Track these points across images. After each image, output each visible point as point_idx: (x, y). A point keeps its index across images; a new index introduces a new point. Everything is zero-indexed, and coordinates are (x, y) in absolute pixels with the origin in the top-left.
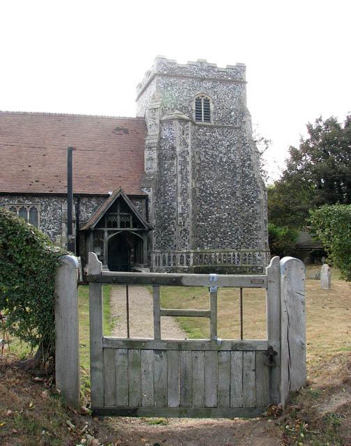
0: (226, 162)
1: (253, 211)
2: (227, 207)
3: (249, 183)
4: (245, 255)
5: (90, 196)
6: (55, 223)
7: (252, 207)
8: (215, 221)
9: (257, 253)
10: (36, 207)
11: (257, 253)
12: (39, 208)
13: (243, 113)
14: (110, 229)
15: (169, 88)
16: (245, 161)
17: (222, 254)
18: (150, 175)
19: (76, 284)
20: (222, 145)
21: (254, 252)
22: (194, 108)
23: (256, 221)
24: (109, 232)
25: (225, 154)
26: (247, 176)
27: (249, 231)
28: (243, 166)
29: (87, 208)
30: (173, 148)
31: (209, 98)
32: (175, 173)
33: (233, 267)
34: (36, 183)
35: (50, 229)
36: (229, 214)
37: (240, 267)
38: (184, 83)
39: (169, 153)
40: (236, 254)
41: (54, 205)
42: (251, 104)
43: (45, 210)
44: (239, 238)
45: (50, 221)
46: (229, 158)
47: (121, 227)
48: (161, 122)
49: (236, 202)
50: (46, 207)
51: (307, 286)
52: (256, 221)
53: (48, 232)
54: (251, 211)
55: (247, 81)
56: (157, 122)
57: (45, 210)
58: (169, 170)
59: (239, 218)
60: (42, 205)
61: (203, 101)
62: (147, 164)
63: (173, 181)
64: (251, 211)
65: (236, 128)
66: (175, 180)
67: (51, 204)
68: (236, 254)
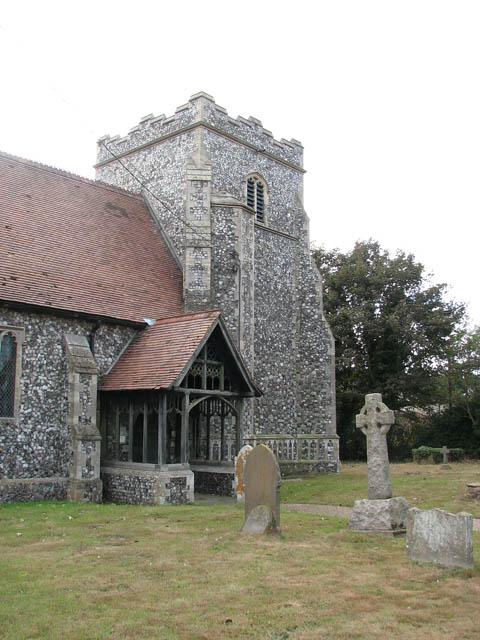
0: (281, 291)
1: (318, 374)
2: (282, 364)
3: (313, 329)
4: (306, 444)
5: (111, 323)
6: (49, 372)
7: (318, 367)
8: (269, 386)
9: (326, 442)
10: (15, 333)
11: (326, 442)
12: (21, 337)
13: (302, 219)
14: (192, 390)
15: (217, 153)
16: (305, 293)
17: (277, 442)
18: (199, 295)
19: (112, 508)
20: (277, 262)
21: (321, 439)
22: (246, 195)
23: (324, 390)
24: (193, 397)
25: (280, 278)
26: (308, 316)
27: (311, 406)
28: (302, 300)
29: (106, 347)
30: (234, 255)
31: (263, 183)
32: (237, 299)
33: (290, 464)
34: (12, 282)
35: (39, 385)
36: (284, 376)
37: (299, 464)
38: (235, 149)
39: (226, 262)
40: (293, 442)
41: (49, 333)
42: (309, 206)
43: (33, 343)
44: (295, 415)
45: (40, 367)
46: (284, 284)
47: (209, 388)
48: (213, 205)
49: (291, 358)
50: (35, 336)
51: (34, 525)
52: (324, 390)
53: (36, 391)
54: (314, 372)
55: (305, 168)
56: (207, 204)
57: (33, 343)
58: (225, 291)
59: (295, 383)
60: (27, 331)
61: (255, 185)
62: (190, 277)
63: (233, 311)
64: (314, 372)
65: (292, 239)
66: (237, 310)
67: (44, 331)
68: (293, 442)
